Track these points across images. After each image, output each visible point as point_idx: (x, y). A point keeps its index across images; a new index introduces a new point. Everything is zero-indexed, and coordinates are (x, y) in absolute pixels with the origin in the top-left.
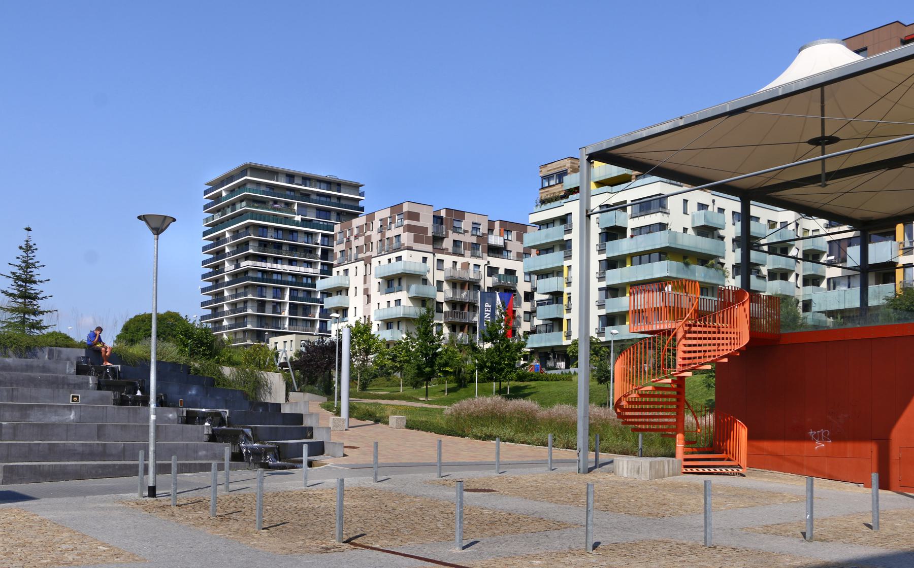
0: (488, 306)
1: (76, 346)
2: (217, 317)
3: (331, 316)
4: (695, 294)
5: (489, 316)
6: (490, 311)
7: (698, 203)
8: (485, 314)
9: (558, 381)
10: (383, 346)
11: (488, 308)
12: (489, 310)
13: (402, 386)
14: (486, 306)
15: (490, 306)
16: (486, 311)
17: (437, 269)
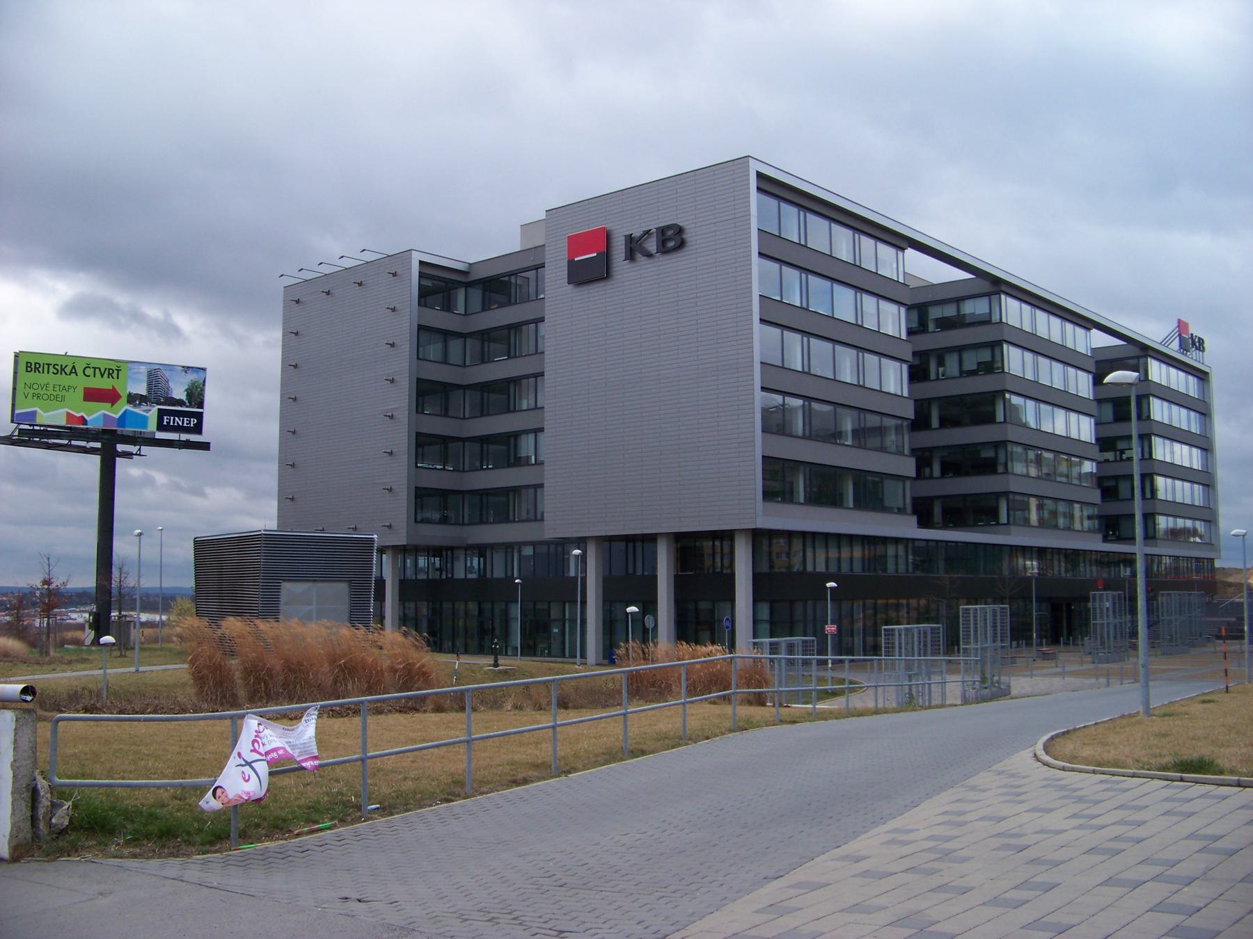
0: (192, 423)
1: (1109, 762)
2: (1036, 601)
3: (1105, 382)
4: (370, 598)
5: (178, 423)
6: (185, 425)
7: (420, 261)
8: (181, 419)
9: (1065, 771)
10: (504, 700)
11: (190, 423)
12: (187, 424)
13: (124, 427)
14: (192, 419)
15: (192, 426)
16: (185, 419)
17: (762, 321)
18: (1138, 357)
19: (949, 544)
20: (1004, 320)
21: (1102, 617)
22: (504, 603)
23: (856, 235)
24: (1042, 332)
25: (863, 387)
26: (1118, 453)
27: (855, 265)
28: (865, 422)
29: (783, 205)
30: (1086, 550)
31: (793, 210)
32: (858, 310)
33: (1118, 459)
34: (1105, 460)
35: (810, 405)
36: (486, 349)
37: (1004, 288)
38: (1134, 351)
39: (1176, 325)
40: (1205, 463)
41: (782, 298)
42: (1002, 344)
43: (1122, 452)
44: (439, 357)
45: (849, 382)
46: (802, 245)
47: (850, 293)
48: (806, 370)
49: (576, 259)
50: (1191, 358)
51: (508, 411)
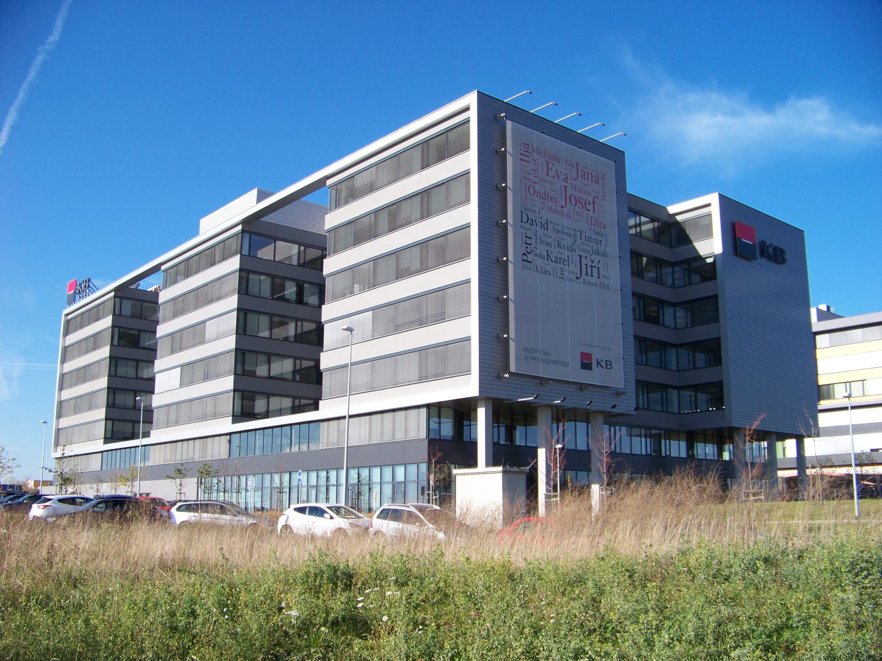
49: (743, 240)
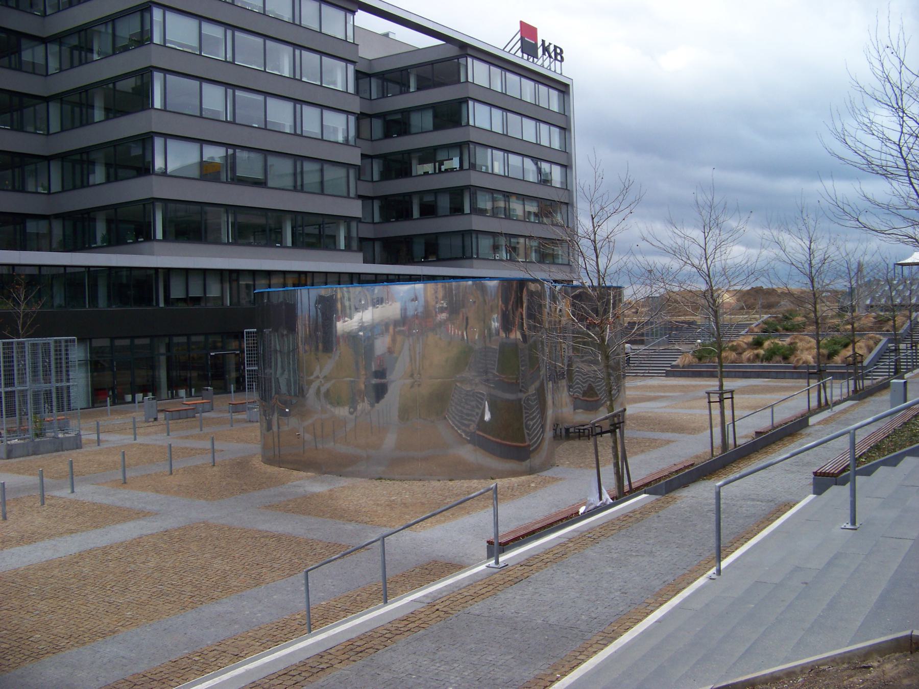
18: (458, 57)
19: (91, 269)
20: (470, 80)
21: (22, 382)
22: (186, 337)
23: (537, 85)
24: (513, 92)
25: (508, 177)
26: (437, 164)
27: (535, 105)
28: (348, 177)
29: (523, 79)
30: (340, 273)
31: (498, 71)
32: (538, 134)
33: (437, 171)
34: (424, 173)
35: (234, 155)
36: (299, 170)
37: (470, 52)
38: (453, 51)
39: (518, 28)
40: (564, 180)
41: (265, 69)
42: (468, 101)
43: (441, 163)
44: (288, 182)
45: (289, 132)
46: (296, 25)
47: (533, 123)
48: (507, 174)
50: (542, 64)
51: (83, 187)
